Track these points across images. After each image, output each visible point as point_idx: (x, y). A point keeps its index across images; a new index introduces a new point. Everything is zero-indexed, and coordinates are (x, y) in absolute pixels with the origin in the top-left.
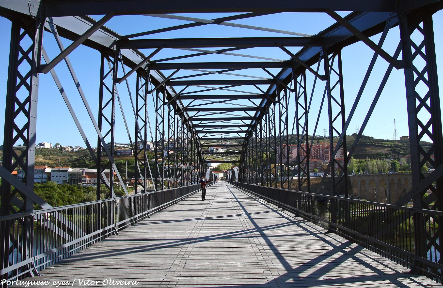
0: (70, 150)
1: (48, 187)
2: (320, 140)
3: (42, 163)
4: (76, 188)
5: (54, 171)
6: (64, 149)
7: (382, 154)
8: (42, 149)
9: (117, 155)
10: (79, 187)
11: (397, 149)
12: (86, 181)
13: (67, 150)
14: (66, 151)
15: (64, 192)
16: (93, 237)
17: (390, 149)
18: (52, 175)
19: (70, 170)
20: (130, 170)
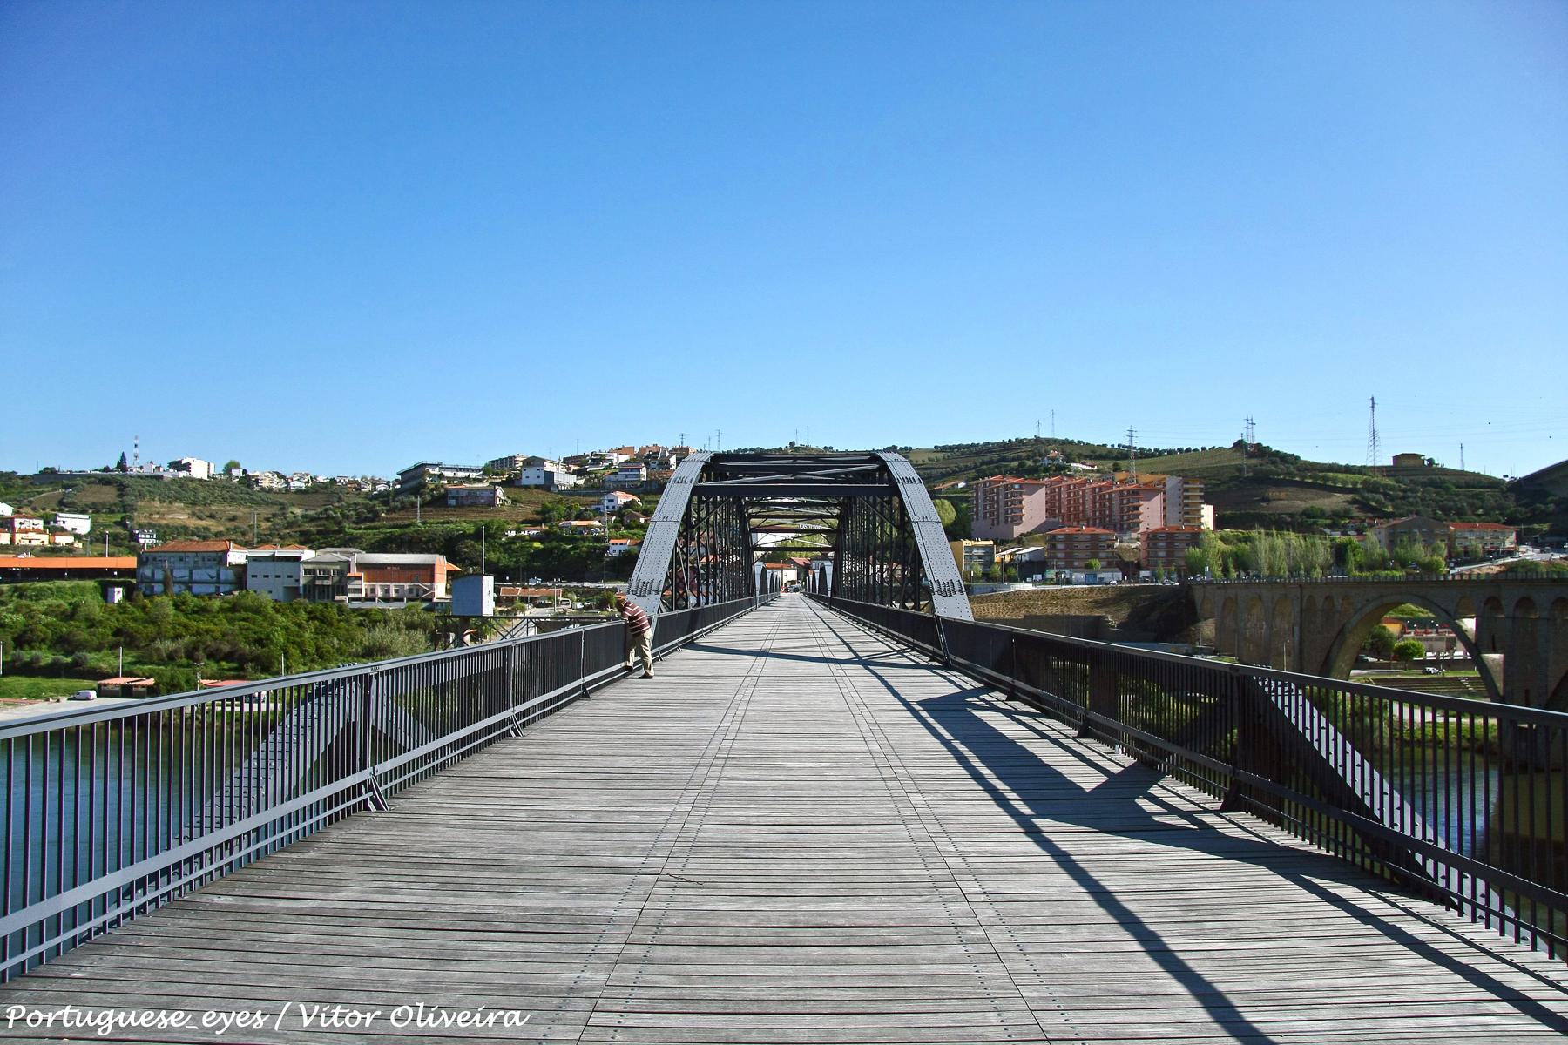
0: (277, 484)
1: (247, 609)
2: (1122, 463)
3: (185, 528)
4: (332, 612)
5: (256, 559)
6: (257, 481)
7: (1322, 514)
8: (183, 483)
9: (447, 506)
10: (341, 610)
11: (1374, 499)
12: (359, 591)
13: (266, 484)
14: (262, 489)
15: (300, 626)
16: (455, 745)
17: (1349, 497)
18: (250, 573)
19: (308, 555)
20: (493, 556)
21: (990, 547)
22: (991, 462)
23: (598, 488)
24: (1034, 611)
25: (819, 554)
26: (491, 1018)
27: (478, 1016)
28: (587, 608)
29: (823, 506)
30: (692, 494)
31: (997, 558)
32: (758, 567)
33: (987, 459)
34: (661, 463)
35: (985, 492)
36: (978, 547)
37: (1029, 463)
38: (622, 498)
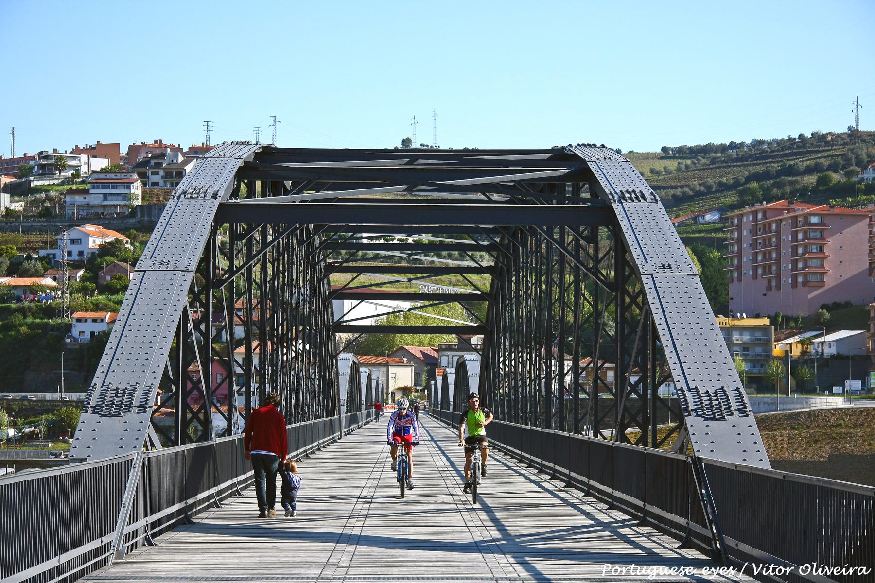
21: (763, 329)
22: (766, 176)
23: (50, 217)
24: (848, 447)
25: (453, 338)
26: (851, 571)
27: (844, 570)
28: (24, 439)
29: (463, 249)
30: (219, 220)
31: (778, 349)
32: (345, 361)
33: (760, 169)
34: (168, 175)
35: (754, 231)
36: (742, 329)
37: (836, 177)
38: (96, 237)
